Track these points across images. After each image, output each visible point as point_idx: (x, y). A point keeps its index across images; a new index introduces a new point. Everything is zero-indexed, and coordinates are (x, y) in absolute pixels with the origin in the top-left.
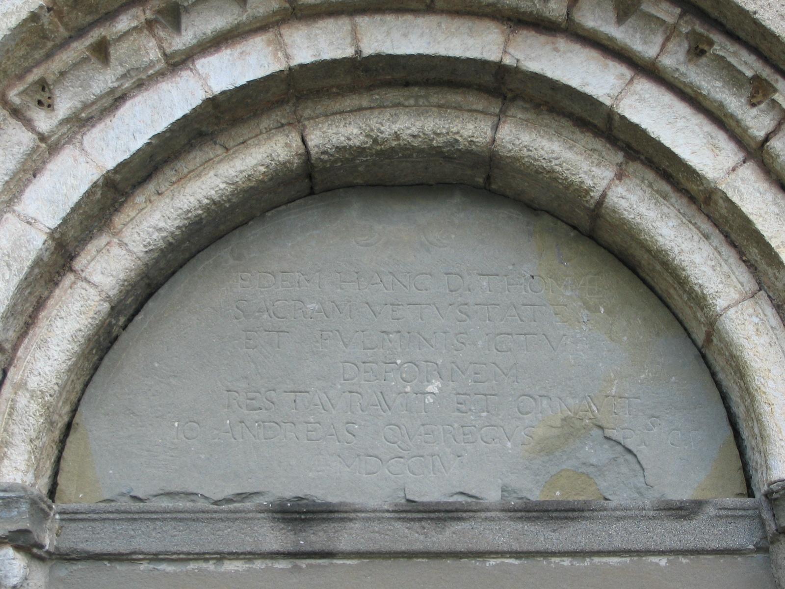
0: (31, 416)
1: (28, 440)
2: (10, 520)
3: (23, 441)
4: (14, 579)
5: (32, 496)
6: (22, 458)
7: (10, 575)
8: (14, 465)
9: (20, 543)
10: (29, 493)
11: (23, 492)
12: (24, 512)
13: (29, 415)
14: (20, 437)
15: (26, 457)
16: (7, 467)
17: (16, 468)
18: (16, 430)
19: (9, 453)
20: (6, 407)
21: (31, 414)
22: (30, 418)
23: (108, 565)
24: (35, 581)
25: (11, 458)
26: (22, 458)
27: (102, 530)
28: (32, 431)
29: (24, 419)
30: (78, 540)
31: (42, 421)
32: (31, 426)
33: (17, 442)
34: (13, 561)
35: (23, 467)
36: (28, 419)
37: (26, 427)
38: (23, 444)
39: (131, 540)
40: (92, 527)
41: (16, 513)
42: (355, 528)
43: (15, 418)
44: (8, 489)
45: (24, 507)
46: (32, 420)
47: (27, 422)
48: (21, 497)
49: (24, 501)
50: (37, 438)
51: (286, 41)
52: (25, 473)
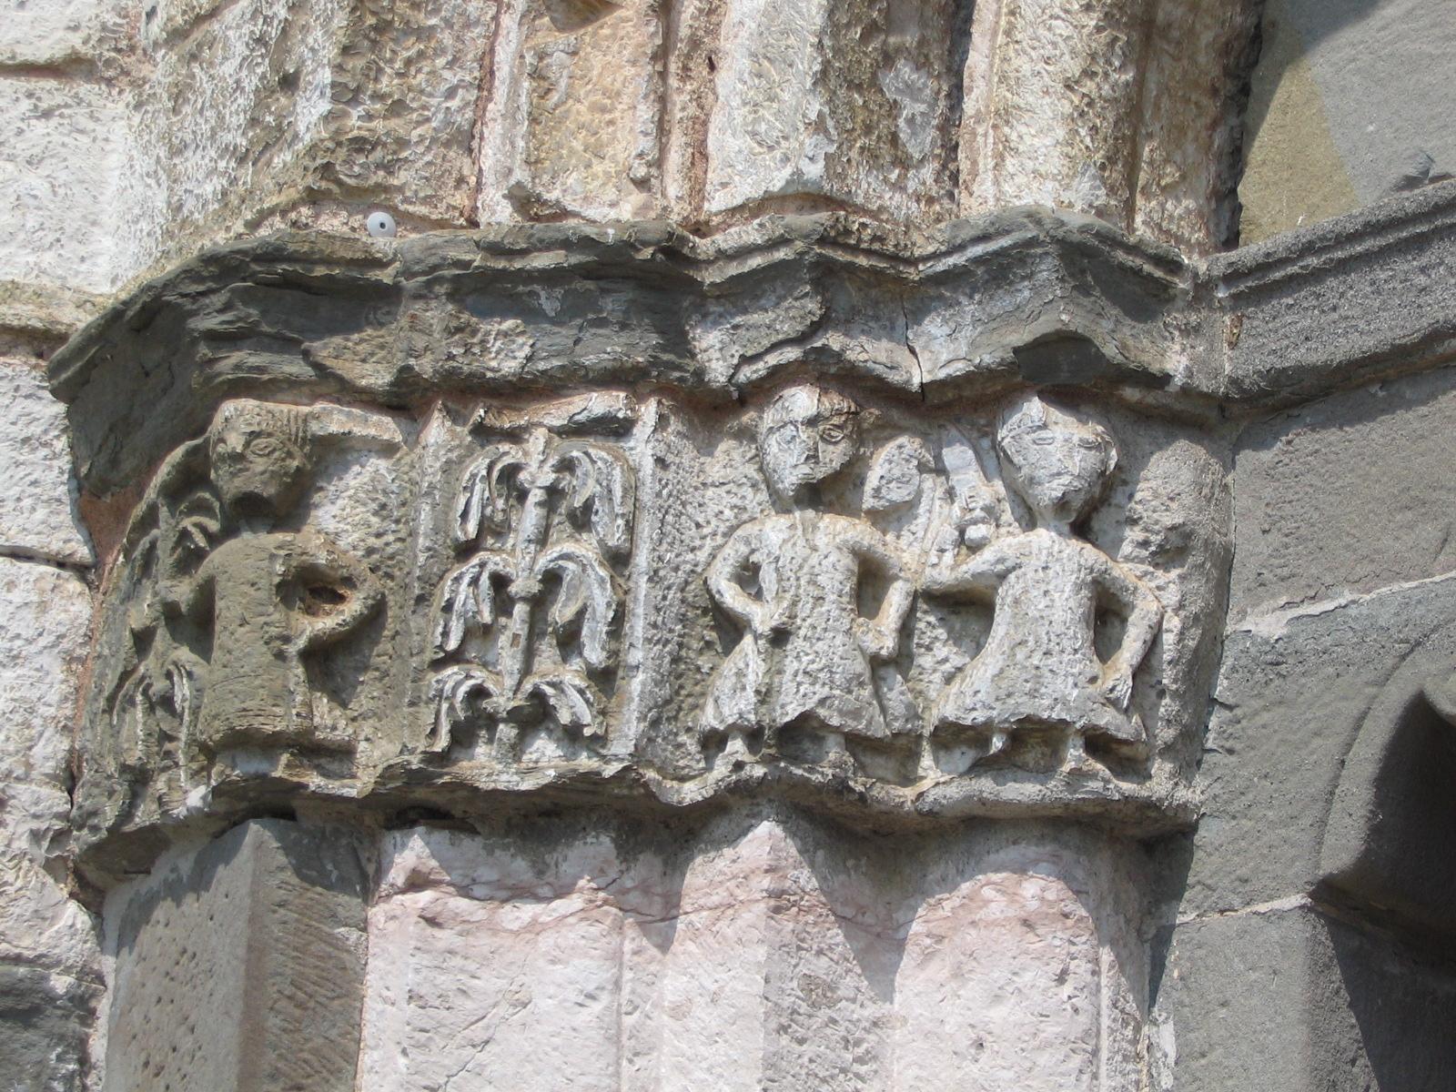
0: (1058, 18)
1: (1060, 87)
2: (1010, 317)
3: (1047, 93)
5: (1060, 233)
6: (1048, 141)
7: (1040, 473)
8: (1030, 165)
9: (1064, 376)
10: (1048, 226)
12: (1047, 284)
13: (1051, 17)
15: (1061, 133)
16: (1012, 176)
17: (1036, 173)
18: (1026, 68)
19: (1014, 136)
20: (998, 14)
21: (1057, 11)
22: (1054, 22)
23: (1381, 394)
24: (1153, 484)
25: (1021, 148)
27: (1342, 295)
28: (1067, 57)
29: (1042, 31)
30: (1286, 342)
31: (1093, 23)
32: (1062, 45)
33: (1031, 99)
34: (1043, 434)
35: (1055, 164)
36: (1050, 29)
37: (1049, 51)
38: (1047, 100)
39: (1421, 301)
40: (1318, 296)
41: (1027, 293)
43: (1019, 37)
44: (992, 230)
45: (1046, 270)
46: (1061, 28)
47: (1050, 36)
48: (1032, 242)
50: (1088, 74)
52: (1065, 181)
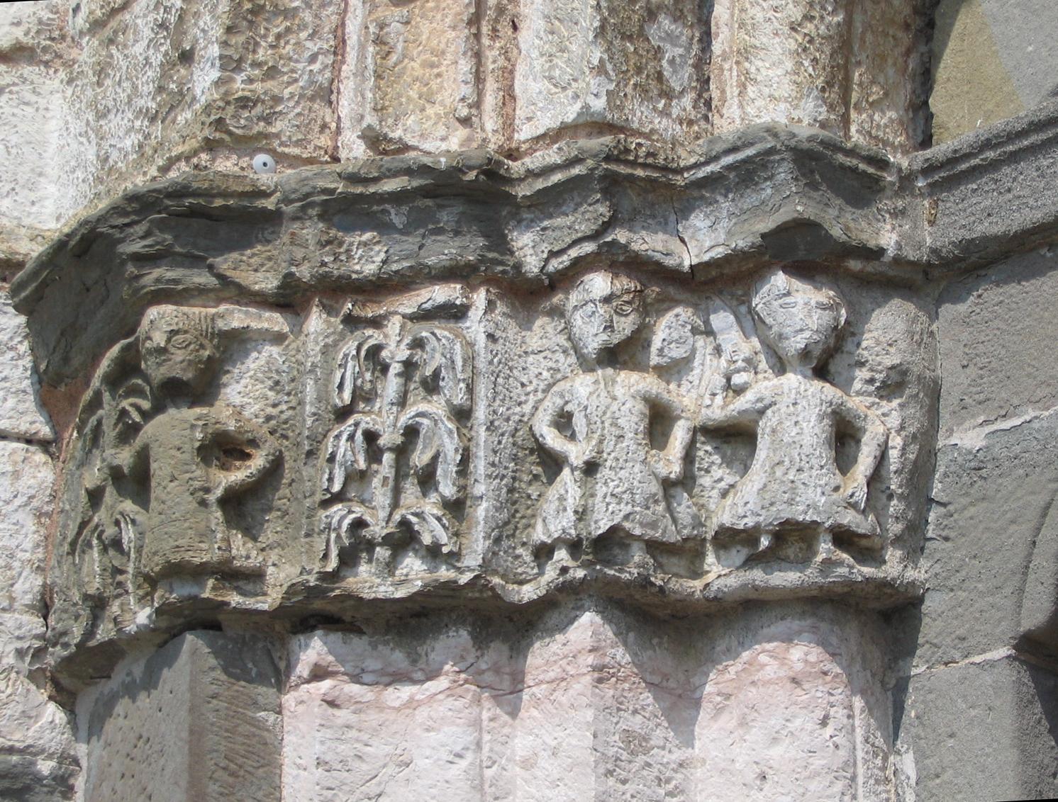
1: (786, 29)
4: (799, 338)
5: (793, 143)
6: (779, 72)
7: (787, 330)
8: (766, 91)
9: (801, 254)
11: (770, 138)
14: (768, 28)
15: (789, 65)
16: (753, 100)
19: (753, 70)
24: (875, 334)
25: (759, 78)
26: (779, 72)
27: (1015, 179)
30: (973, 219)
33: (765, 40)
34: (788, 300)
35: (786, 89)
38: (777, 40)
40: (996, 181)
41: (769, 191)
42: (295, 28)
44: (739, 143)
45: (783, 172)
48: (772, 151)
49: (777, 157)
50: (808, 18)
51: (23, 251)
52: (795, 102)
